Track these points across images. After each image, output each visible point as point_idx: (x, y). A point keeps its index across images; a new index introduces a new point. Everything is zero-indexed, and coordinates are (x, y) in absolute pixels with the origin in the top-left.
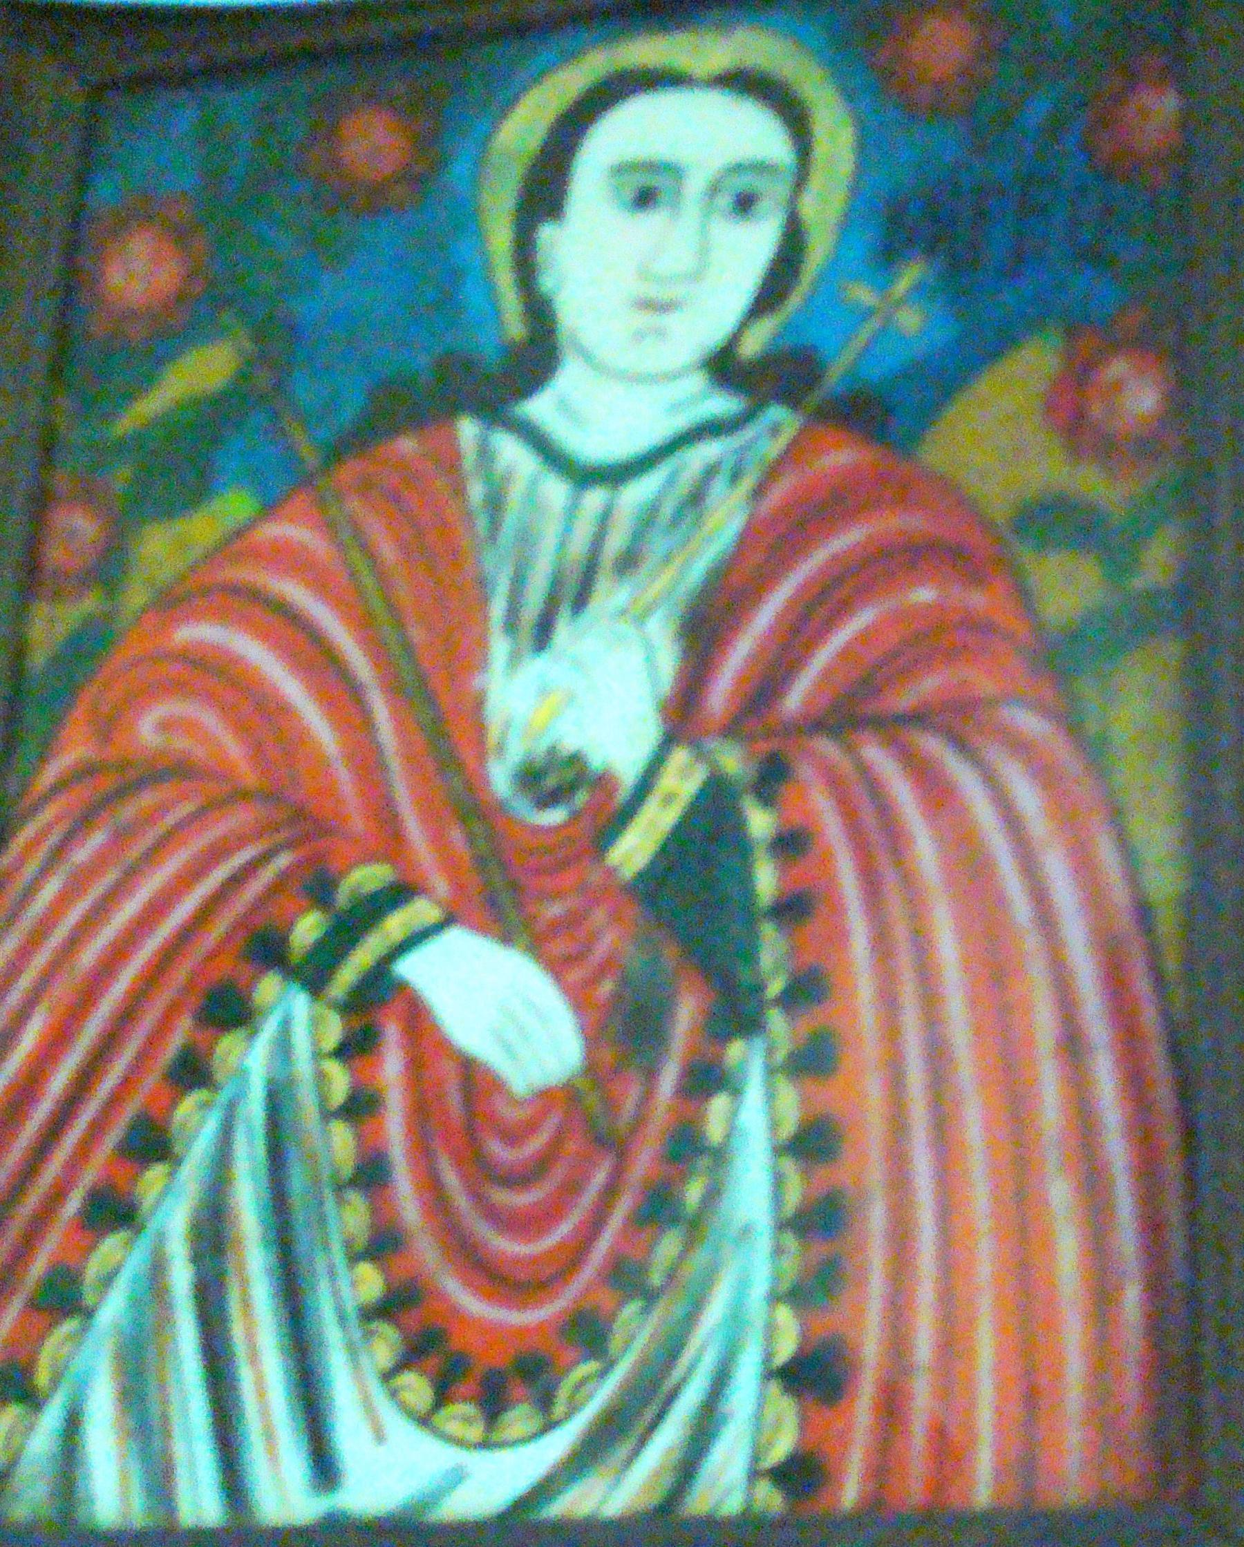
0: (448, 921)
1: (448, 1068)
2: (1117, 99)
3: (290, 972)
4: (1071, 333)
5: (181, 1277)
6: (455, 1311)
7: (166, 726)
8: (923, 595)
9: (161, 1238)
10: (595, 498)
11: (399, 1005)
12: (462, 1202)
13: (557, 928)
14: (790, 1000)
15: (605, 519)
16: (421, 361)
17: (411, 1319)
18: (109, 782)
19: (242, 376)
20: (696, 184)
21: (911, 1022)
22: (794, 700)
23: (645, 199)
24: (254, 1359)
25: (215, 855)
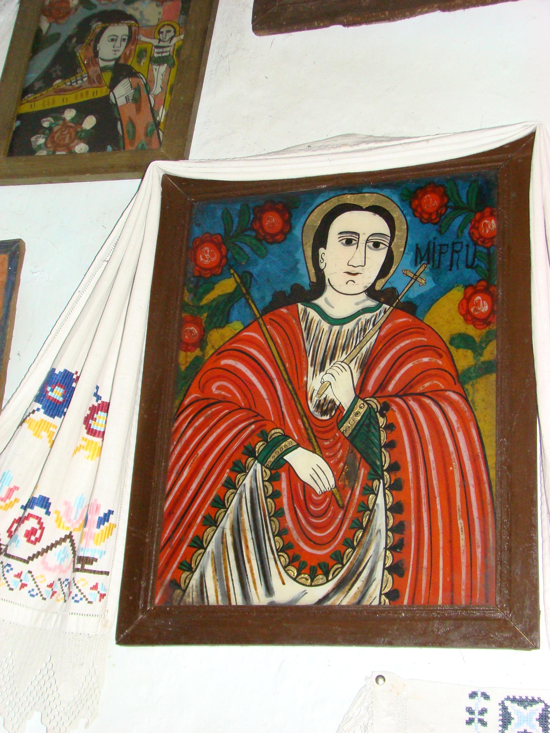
0: (298, 446)
1: (318, 452)
2: (479, 221)
3: (256, 458)
4: (466, 287)
5: (229, 540)
6: (302, 550)
7: (218, 388)
8: (426, 360)
9: (223, 529)
10: (336, 328)
11: (286, 466)
12: (303, 521)
13: (328, 448)
14: (389, 470)
15: (339, 333)
16: (287, 289)
17: (290, 552)
18: (204, 403)
19: (237, 288)
20: (363, 239)
21: (422, 477)
22: (390, 388)
23: (349, 242)
24: (249, 561)
25: (234, 425)
